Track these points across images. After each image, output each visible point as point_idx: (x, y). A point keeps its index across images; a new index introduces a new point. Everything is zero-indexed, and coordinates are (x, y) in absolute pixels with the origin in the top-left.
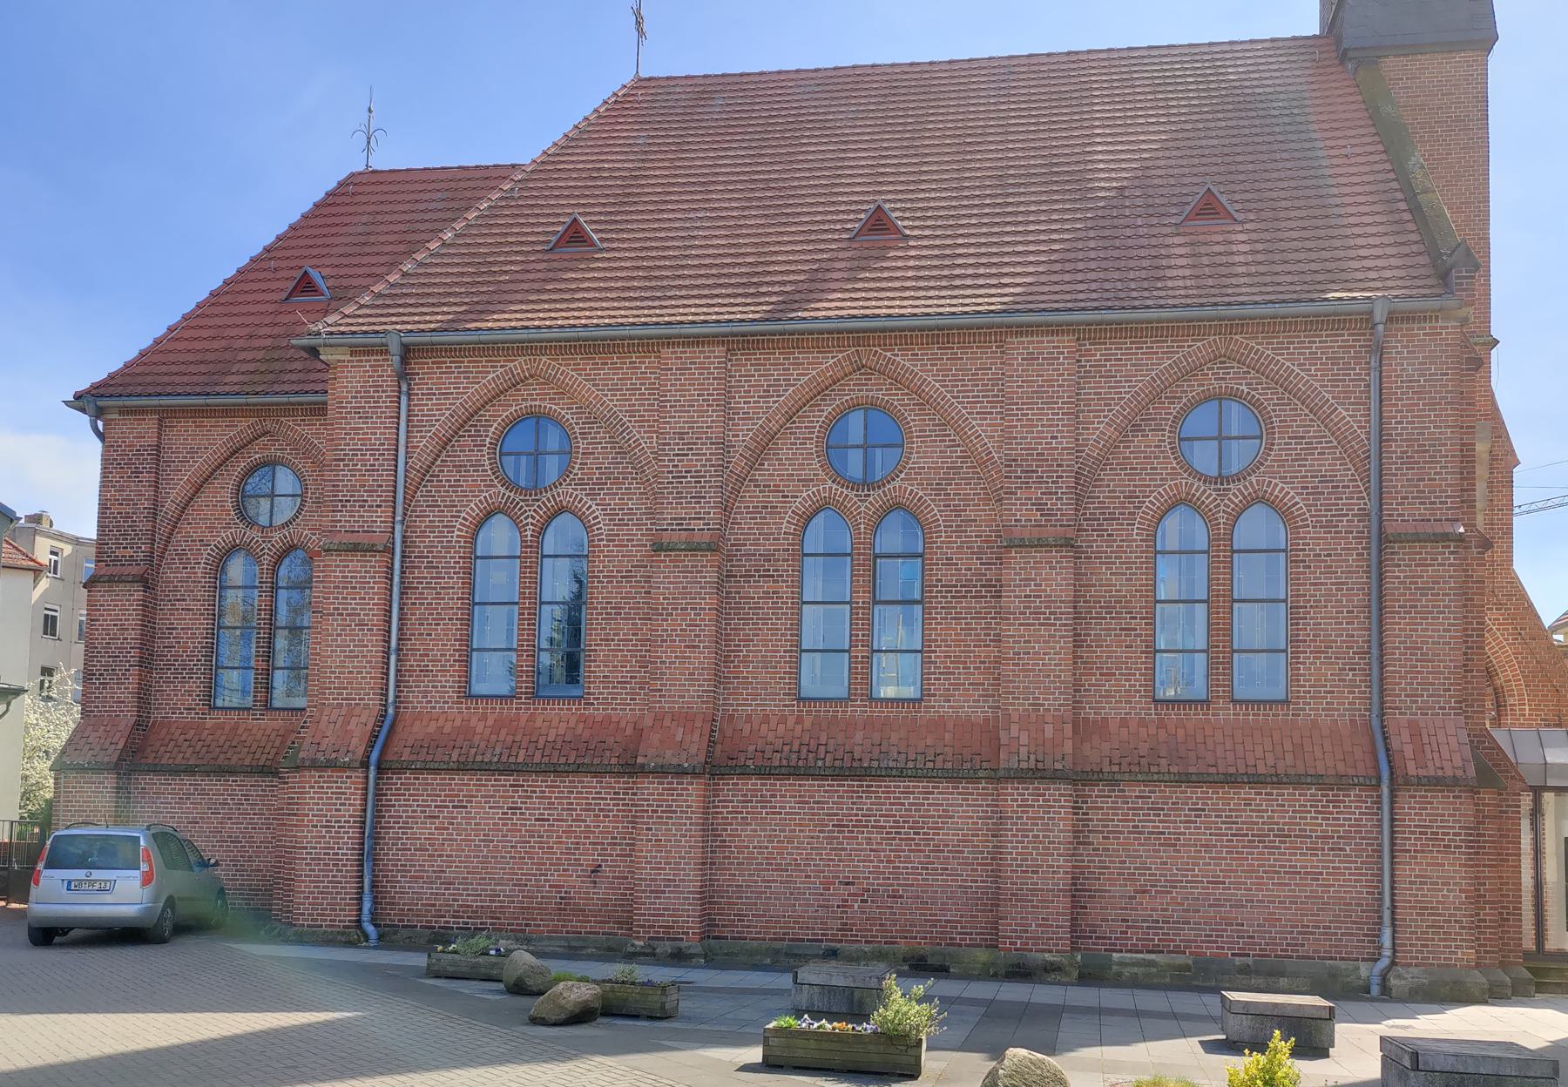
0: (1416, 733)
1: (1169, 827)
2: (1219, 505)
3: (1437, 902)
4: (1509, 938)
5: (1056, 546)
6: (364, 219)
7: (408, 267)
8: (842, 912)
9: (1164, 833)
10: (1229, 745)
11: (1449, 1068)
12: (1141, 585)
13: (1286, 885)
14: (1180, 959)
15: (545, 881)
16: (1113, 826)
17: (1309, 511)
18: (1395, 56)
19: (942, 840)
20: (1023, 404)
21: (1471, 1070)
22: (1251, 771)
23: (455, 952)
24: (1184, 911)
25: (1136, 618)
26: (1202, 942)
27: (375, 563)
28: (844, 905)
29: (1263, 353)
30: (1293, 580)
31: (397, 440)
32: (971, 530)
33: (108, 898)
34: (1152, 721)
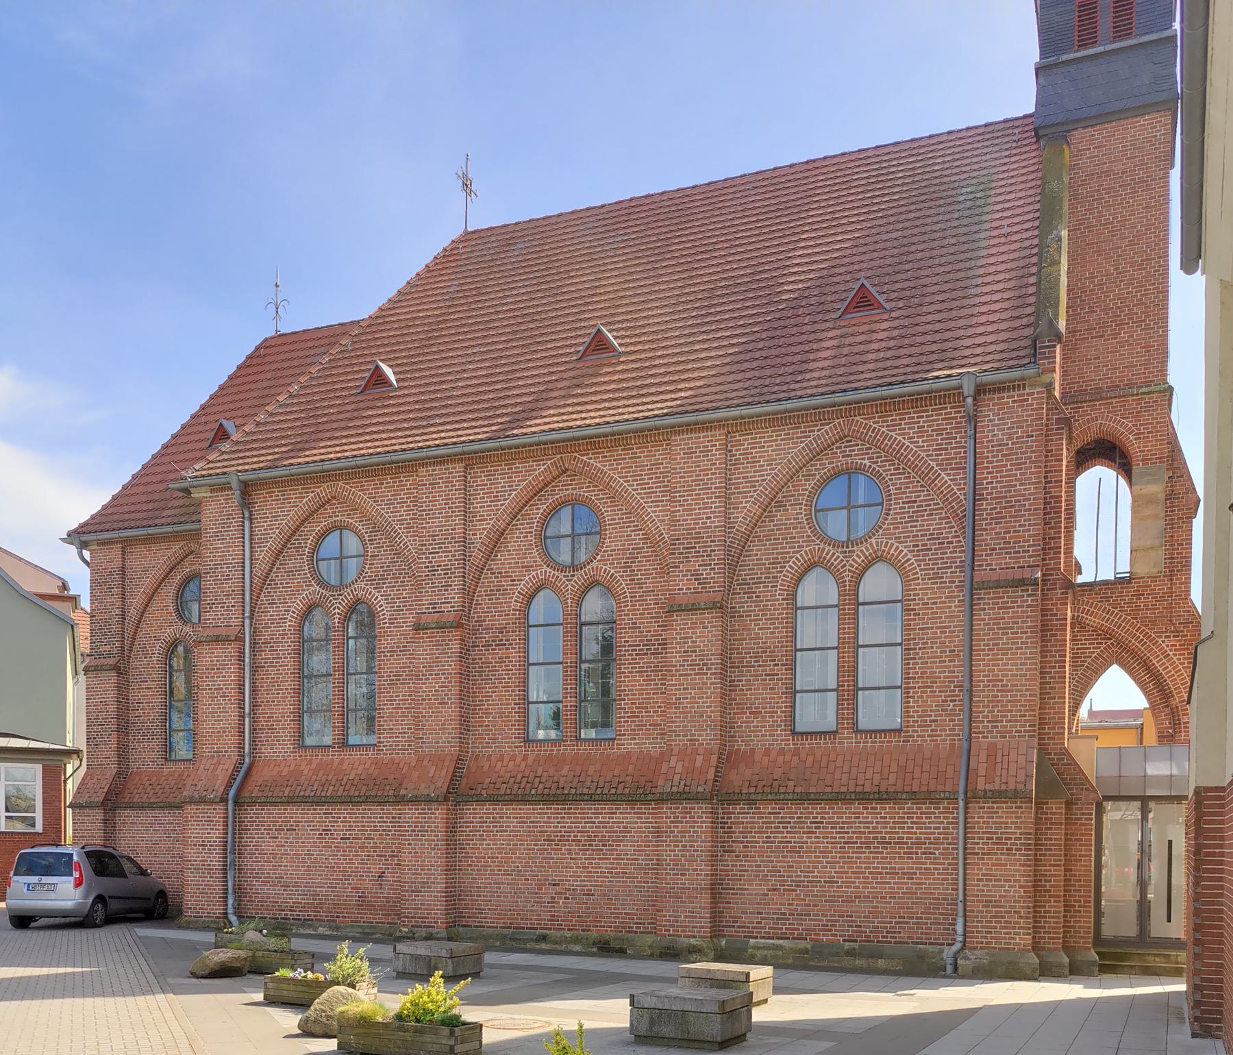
0: (992, 752)
1: (794, 837)
2: (845, 565)
3: (1000, 896)
4: (1080, 927)
5: (707, 609)
6: (269, 375)
7: (261, 417)
8: (551, 907)
9: (790, 842)
10: (878, 769)
11: (653, 1006)
12: (782, 637)
13: (887, 883)
14: (802, 944)
15: (349, 884)
16: (751, 837)
17: (919, 565)
18: (1084, 128)
19: (622, 850)
20: (684, 491)
21: (666, 1007)
22: (859, 789)
23: (231, 933)
24: (806, 905)
25: (778, 665)
26: (820, 930)
27: (232, 649)
28: (552, 901)
29: (879, 430)
30: (906, 627)
31: (244, 555)
32: (650, 599)
33: (52, 895)
34: (790, 750)
